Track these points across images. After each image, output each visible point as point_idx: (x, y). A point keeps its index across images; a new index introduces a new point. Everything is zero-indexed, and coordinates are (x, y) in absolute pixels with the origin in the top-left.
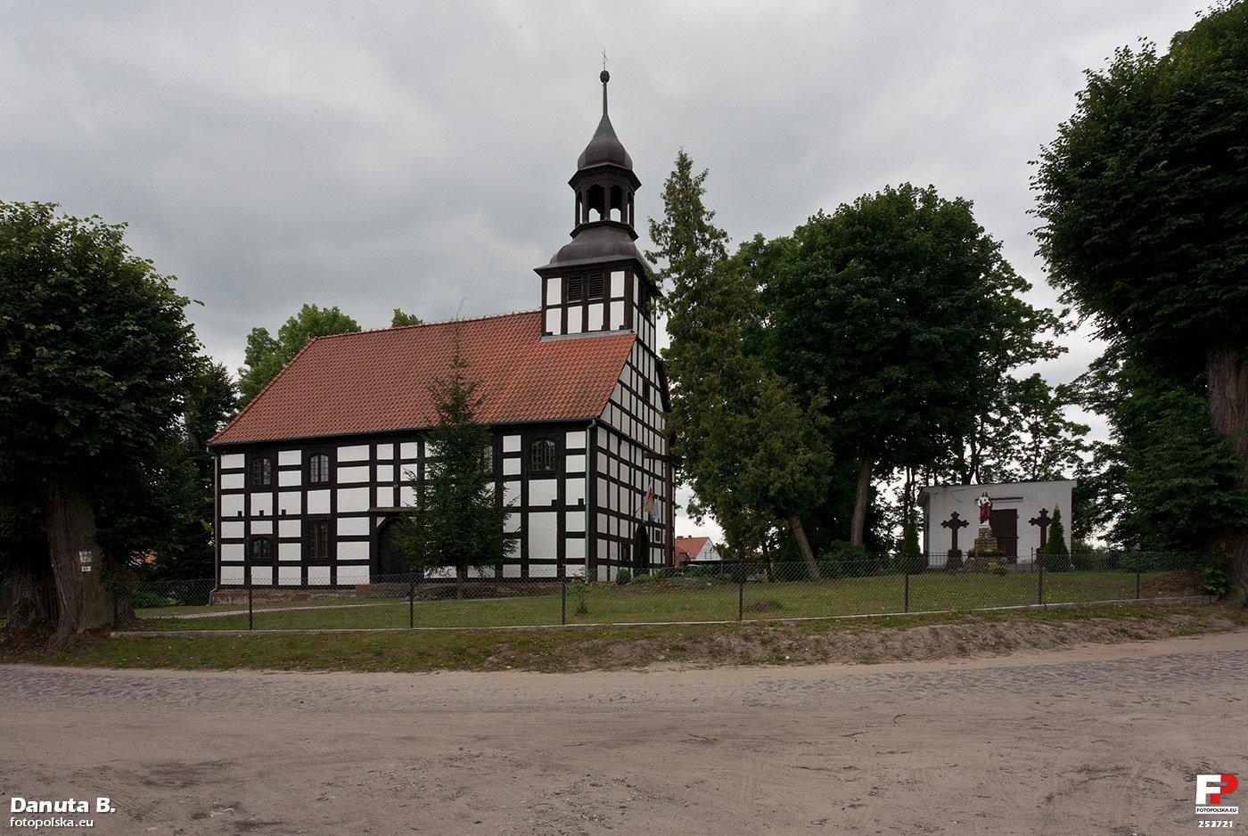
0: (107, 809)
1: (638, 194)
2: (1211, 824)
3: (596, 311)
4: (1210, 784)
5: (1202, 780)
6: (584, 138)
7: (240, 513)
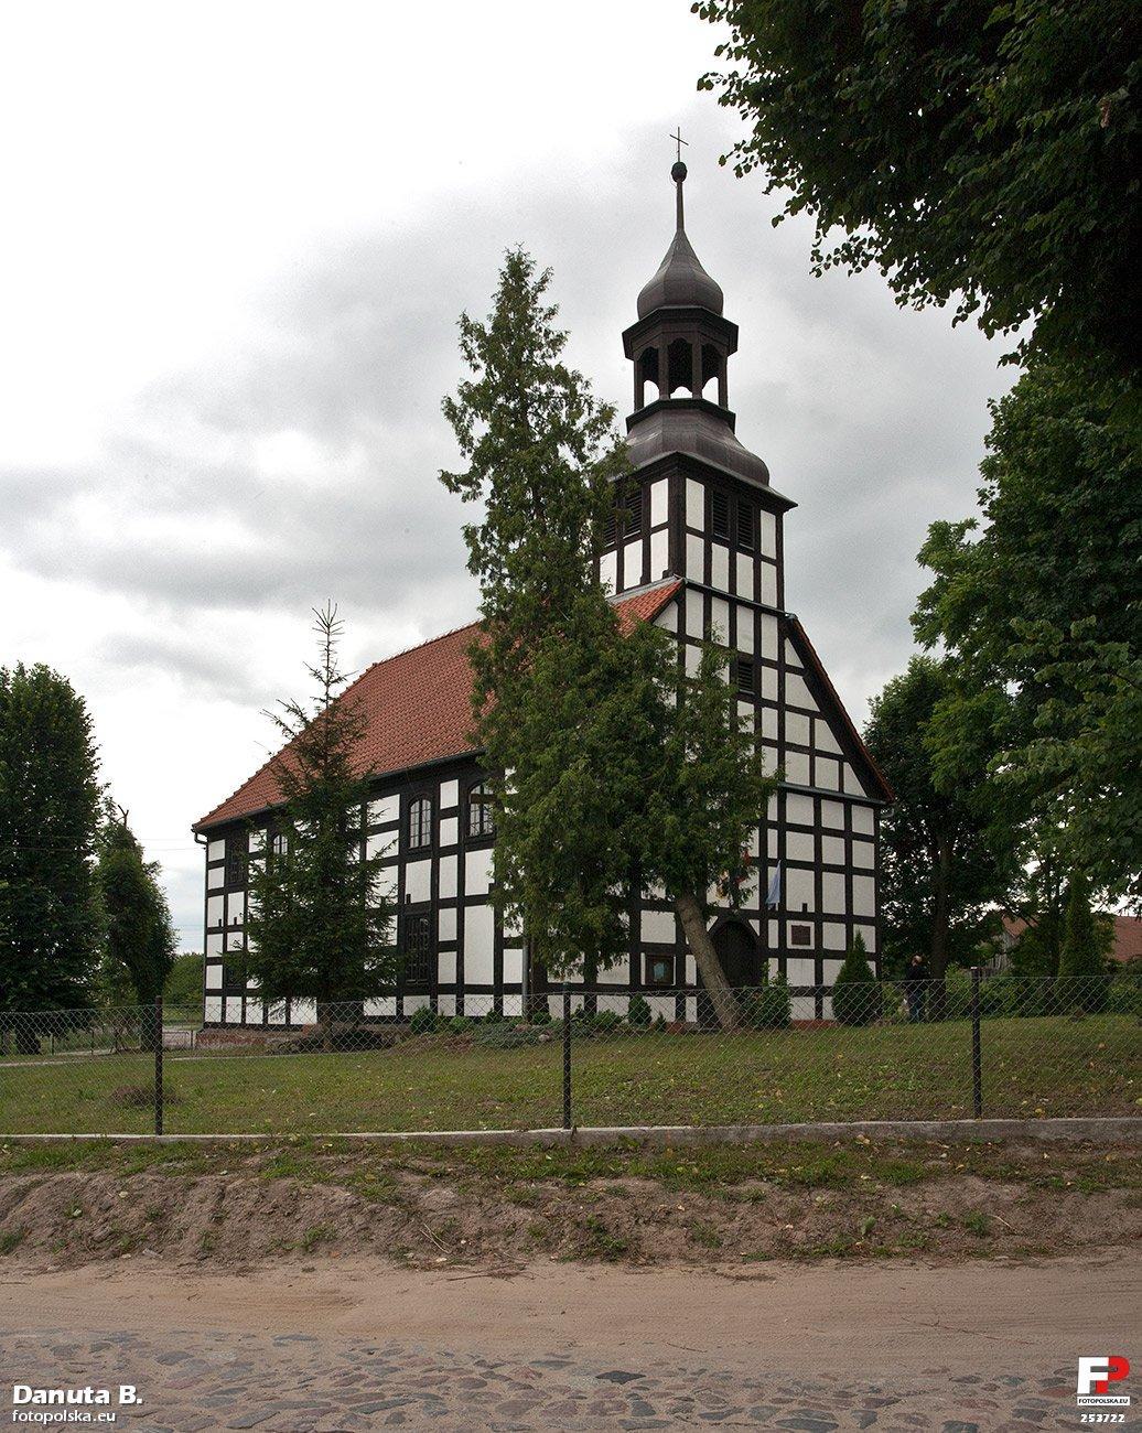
0: (132, 1400)
2: (1096, 1418)
3: (634, 551)
4: (1094, 1369)
5: (1085, 1364)
6: (647, 268)
7: (805, 906)
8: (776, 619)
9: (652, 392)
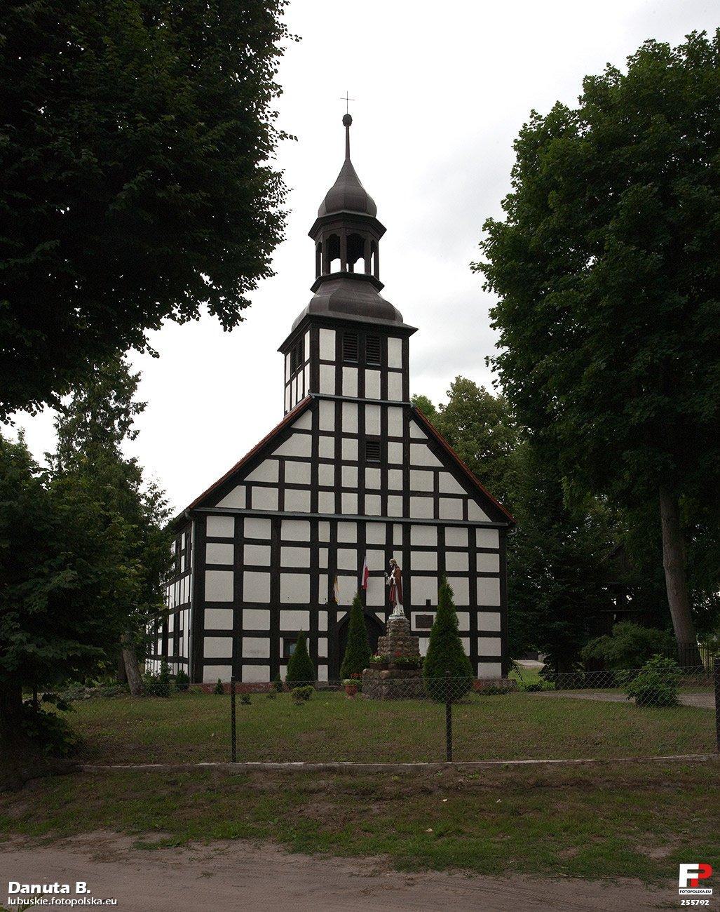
1: (383, 244)
4: (690, 871)
5: (684, 868)
8: (357, 405)
9: (336, 266)
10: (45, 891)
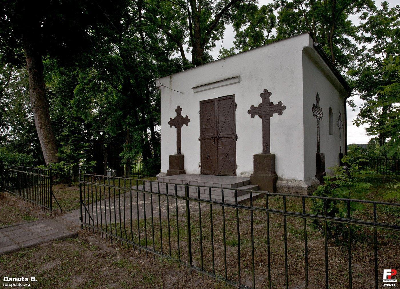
0: (34, 280)
2: (388, 285)
4: (388, 272)
5: (385, 271)
10: (18, 281)
